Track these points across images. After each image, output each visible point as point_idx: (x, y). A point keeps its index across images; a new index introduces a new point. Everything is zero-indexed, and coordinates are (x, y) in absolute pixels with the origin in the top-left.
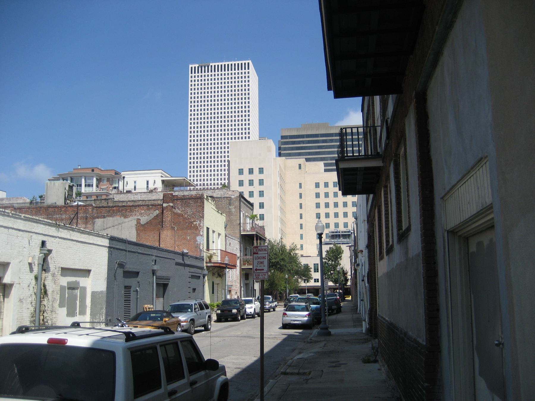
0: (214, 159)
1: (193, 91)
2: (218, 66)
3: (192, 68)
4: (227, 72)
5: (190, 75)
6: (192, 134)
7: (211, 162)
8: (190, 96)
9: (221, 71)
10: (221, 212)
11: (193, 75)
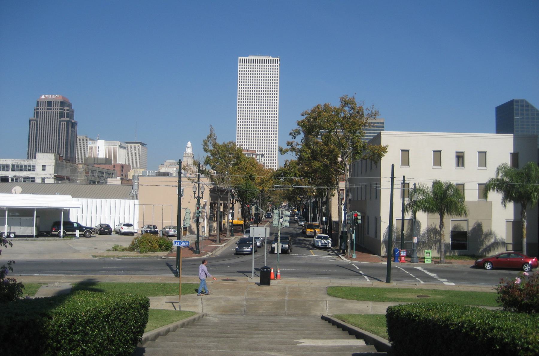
2: (244, 59)
3: (240, 59)
4: (263, 64)
5: (239, 64)
9: (244, 63)
10: (47, 181)
11: (241, 64)
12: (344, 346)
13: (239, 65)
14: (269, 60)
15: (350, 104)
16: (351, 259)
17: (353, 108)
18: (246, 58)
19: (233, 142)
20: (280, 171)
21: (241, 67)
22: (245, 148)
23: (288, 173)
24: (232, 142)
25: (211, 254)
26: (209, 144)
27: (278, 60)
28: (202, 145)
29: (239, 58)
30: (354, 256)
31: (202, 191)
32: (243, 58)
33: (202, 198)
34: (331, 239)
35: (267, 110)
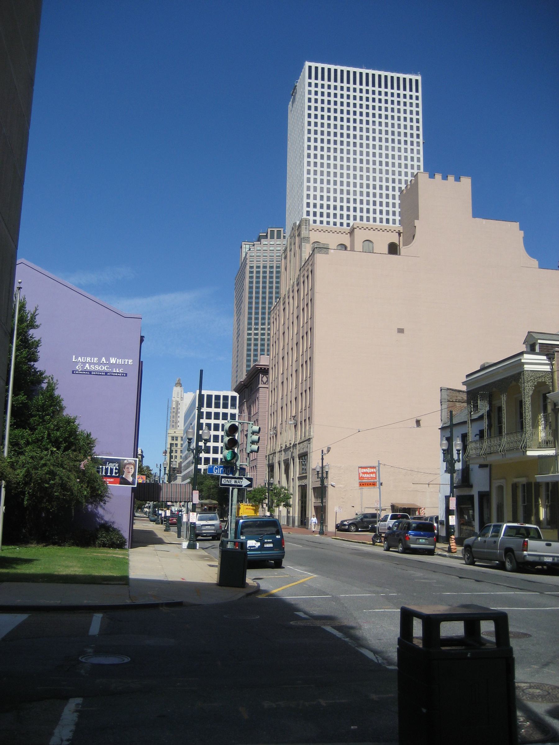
3: (310, 67)
12: (465, 614)
27: (417, 81)
29: (307, 64)
33: (327, 477)
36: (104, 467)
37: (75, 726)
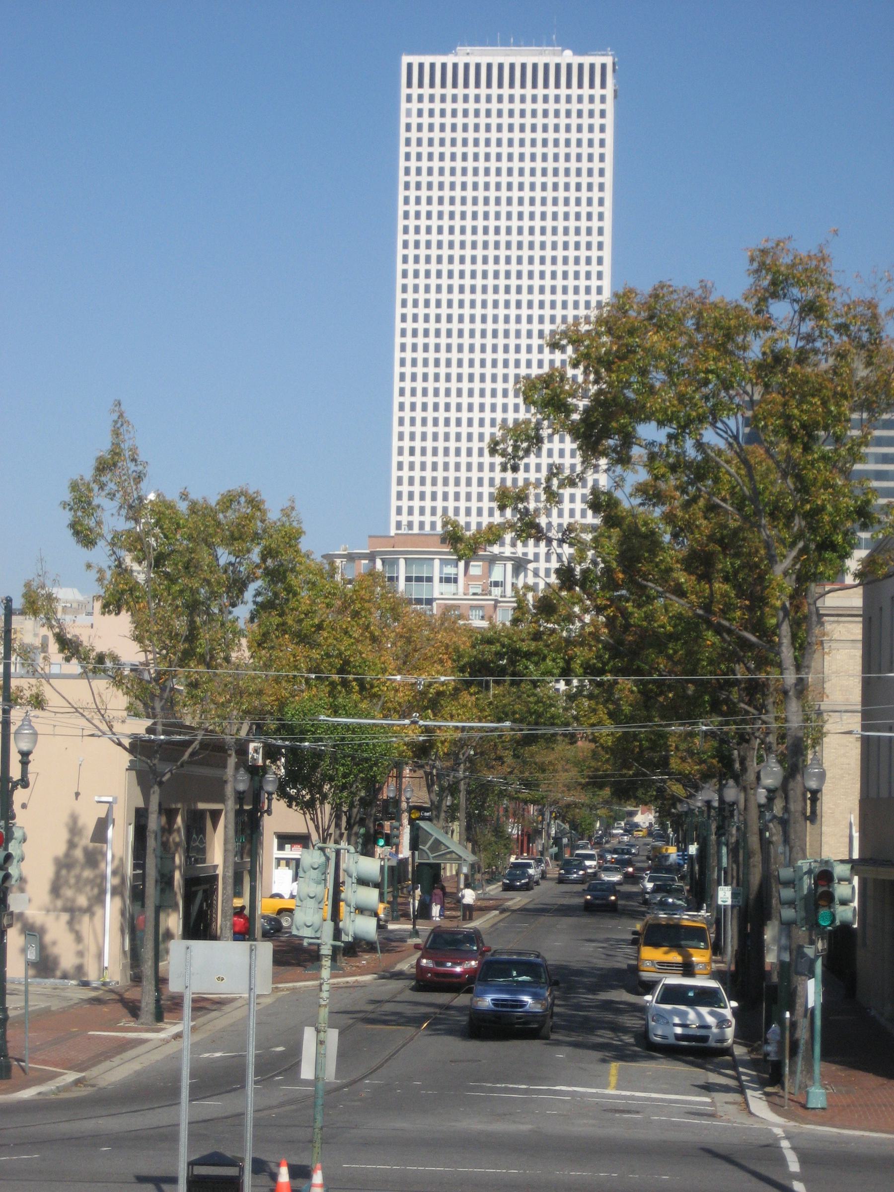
0: (566, 194)
1: (414, 149)
3: (410, 66)
5: (404, 91)
6: (410, 296)
7: (555, 187)
8: (400, 267)
11: (415, 91)
13: (403, 98)
14: (558, 66)
15: (799, 283)
16: (801, 1111)
17: (811, 309)
18: (439, 60)
19: (251, 491)
20: (490, 642)
21: (415, 106)
22: (427, 528)
23: (528, 655)
24: (243, 493)
25: (71, 1077)
26: (99, 499)
27: (604, 66)
28: (65, 505)
29: (406, 59)
30: (817, 1096)
31: (25, 747)
32: (427, 60)
33: (24, 782)
34: (734, 1004)
35: (513, 326)
36: (405, 852)
37: (345, 571)
